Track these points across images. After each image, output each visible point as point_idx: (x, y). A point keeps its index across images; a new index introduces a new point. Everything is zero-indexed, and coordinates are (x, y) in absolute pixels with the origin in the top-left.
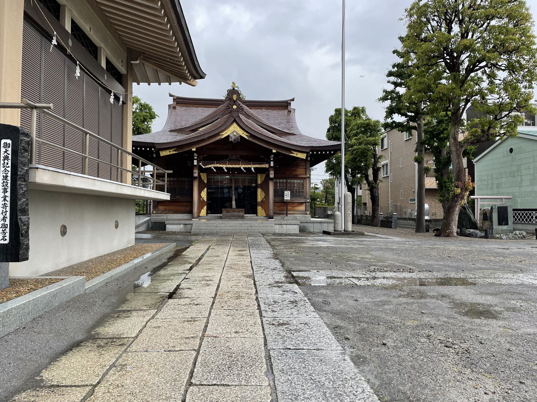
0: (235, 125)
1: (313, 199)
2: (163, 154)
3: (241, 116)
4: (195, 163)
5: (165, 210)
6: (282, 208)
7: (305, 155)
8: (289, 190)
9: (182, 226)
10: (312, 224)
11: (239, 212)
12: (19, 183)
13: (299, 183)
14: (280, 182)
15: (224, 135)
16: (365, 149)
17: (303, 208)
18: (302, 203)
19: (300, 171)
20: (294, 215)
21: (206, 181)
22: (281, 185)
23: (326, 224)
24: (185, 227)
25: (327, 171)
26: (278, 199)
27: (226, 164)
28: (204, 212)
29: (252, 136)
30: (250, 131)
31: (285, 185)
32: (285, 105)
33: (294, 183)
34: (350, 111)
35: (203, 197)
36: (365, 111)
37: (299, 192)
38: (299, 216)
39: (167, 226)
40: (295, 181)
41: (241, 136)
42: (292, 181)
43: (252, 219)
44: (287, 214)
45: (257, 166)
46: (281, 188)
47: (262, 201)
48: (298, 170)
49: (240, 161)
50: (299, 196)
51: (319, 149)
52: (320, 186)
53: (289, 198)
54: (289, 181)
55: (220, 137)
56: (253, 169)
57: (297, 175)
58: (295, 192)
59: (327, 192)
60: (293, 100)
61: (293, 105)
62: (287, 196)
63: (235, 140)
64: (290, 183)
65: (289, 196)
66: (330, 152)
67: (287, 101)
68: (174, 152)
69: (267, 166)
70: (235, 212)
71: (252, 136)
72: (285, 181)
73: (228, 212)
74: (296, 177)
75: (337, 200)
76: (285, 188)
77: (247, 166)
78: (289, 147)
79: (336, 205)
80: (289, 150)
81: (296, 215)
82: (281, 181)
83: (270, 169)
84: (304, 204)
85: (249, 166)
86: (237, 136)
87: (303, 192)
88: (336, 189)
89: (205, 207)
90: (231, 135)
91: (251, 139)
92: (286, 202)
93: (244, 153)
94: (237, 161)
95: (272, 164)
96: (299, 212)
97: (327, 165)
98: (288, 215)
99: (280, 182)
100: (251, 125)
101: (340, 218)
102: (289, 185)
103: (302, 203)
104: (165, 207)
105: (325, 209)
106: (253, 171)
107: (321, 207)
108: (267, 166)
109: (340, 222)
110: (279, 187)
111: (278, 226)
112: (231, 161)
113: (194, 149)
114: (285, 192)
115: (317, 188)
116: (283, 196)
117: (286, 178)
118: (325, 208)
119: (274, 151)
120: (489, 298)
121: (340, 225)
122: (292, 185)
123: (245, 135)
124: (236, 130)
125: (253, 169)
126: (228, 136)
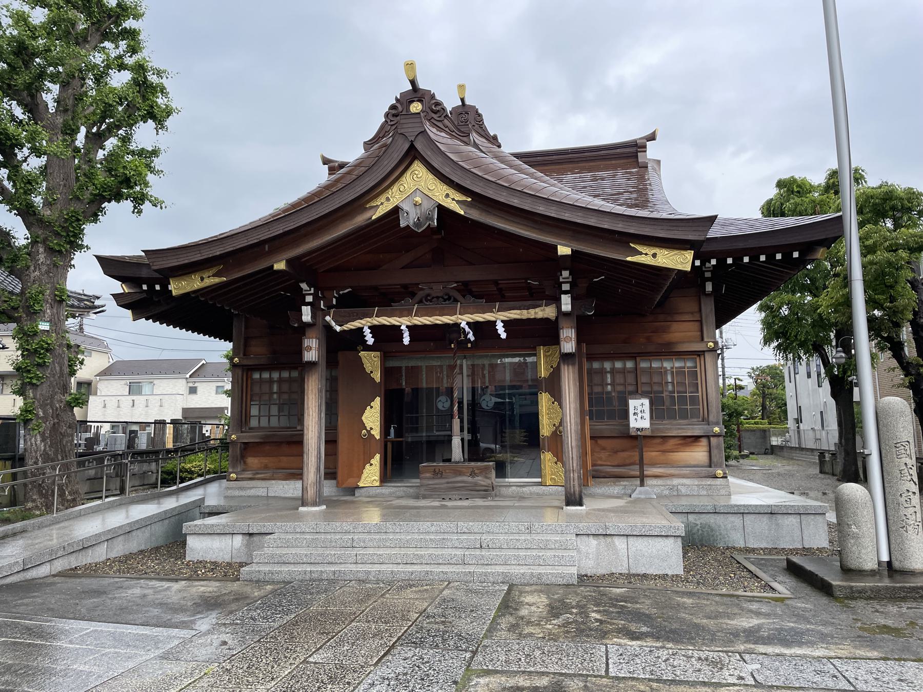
0: (418, 168)
1: (732, 415)
2: (177, 287)
3: (432, 132)
4: (307, 314)
5: (266, 467)
6: (618, 455)
7: (689, 255)
8: (644, 395)
9: (238, 541)
10: (737, 520)
11: (473, 474)
13: (680, 372)
14: (613, 371)
15: (381, 207)
16: (890, 264)
17: (699, 454)
18: (697, 438)
19: (681, 332)
20: (669, 482)
21: (377, 376)
22: (619, 379)
23: (793, 520)
24: (248, 546)
25: (767, 341)
26: (607, 426)
27: (409, 314)
28: (371, 473)
29: (479, 200)
30: (467, 184)
31: (630, 379)
32: (628, 156)
33: (662, 372)
34: (819, 185)
35: (368, 425)
36: (862, 177)
37: (683, 400)
38: (686, 485)
39: (191, 542)
40: (667, 365)
41: (441, 208)
42: (655, 365)
43: (522, 498)
44: (642, 478)
45: (514, 314)
48: (675, 326)
49: (456, 301)
50: (684, 415)
51: (741, 245)
52: (749, 384)
53: (645, 423)
54: (644, 365)
55: (366, 216)
56: (500, 328)
57: (669, 344)
58: (667, 402)
59: (764, 396)
60: (652, 137)
61: (652, 152)
62: (640, 415)
63: (418, 224)
64: (650, 371)
65: (647, 415)
66: (787, 256)
67: (635, 141)
68: (217, 280)
69: (547, 312)
70: (461, 473)
71: (479, 200)
72: (630, 364)
73: (437, 474)
74: (668, 351)
75: (792, 413)
76: (631, 388)
77: (479, 317)
78: (620, 227)
79: (791, 424)
80: (624, 240)
81: (676, 481)
82: (618, 365)
83: (562, 322)
84: (704, 442)
85: (489, 317)
86: (427, 205)
87: (694, 401)
88: (789, 387)
89: (376, 460)
90: (406, 207)
91: (475, 215)
93: (469, 274)
94: (447, 302)
95: (566, 303)
96: (686, 471)
97: (767, 325)
98: (649, 482)
100: (468, 159)
101: (865, 515)
102: (644, 379)
103: (697, 438)
104: (265, 460)
105: (765, 434)
106: (503, 336)
107: (753, 431)
108: (547, 312)
109: (866, 529)
111: (593, 542)
112: (429, 303)
113: (280, 266)
114: (633, 403)
115: (741, 388)
116: (625, 414)
117: (633, 357)
118: (764, 431)
119: (564, 250)
121: (868, 542)
122: (656, 379)
123: (453, 202)
124: (422, 186)
125: (500, 328)
126: (396, 210)
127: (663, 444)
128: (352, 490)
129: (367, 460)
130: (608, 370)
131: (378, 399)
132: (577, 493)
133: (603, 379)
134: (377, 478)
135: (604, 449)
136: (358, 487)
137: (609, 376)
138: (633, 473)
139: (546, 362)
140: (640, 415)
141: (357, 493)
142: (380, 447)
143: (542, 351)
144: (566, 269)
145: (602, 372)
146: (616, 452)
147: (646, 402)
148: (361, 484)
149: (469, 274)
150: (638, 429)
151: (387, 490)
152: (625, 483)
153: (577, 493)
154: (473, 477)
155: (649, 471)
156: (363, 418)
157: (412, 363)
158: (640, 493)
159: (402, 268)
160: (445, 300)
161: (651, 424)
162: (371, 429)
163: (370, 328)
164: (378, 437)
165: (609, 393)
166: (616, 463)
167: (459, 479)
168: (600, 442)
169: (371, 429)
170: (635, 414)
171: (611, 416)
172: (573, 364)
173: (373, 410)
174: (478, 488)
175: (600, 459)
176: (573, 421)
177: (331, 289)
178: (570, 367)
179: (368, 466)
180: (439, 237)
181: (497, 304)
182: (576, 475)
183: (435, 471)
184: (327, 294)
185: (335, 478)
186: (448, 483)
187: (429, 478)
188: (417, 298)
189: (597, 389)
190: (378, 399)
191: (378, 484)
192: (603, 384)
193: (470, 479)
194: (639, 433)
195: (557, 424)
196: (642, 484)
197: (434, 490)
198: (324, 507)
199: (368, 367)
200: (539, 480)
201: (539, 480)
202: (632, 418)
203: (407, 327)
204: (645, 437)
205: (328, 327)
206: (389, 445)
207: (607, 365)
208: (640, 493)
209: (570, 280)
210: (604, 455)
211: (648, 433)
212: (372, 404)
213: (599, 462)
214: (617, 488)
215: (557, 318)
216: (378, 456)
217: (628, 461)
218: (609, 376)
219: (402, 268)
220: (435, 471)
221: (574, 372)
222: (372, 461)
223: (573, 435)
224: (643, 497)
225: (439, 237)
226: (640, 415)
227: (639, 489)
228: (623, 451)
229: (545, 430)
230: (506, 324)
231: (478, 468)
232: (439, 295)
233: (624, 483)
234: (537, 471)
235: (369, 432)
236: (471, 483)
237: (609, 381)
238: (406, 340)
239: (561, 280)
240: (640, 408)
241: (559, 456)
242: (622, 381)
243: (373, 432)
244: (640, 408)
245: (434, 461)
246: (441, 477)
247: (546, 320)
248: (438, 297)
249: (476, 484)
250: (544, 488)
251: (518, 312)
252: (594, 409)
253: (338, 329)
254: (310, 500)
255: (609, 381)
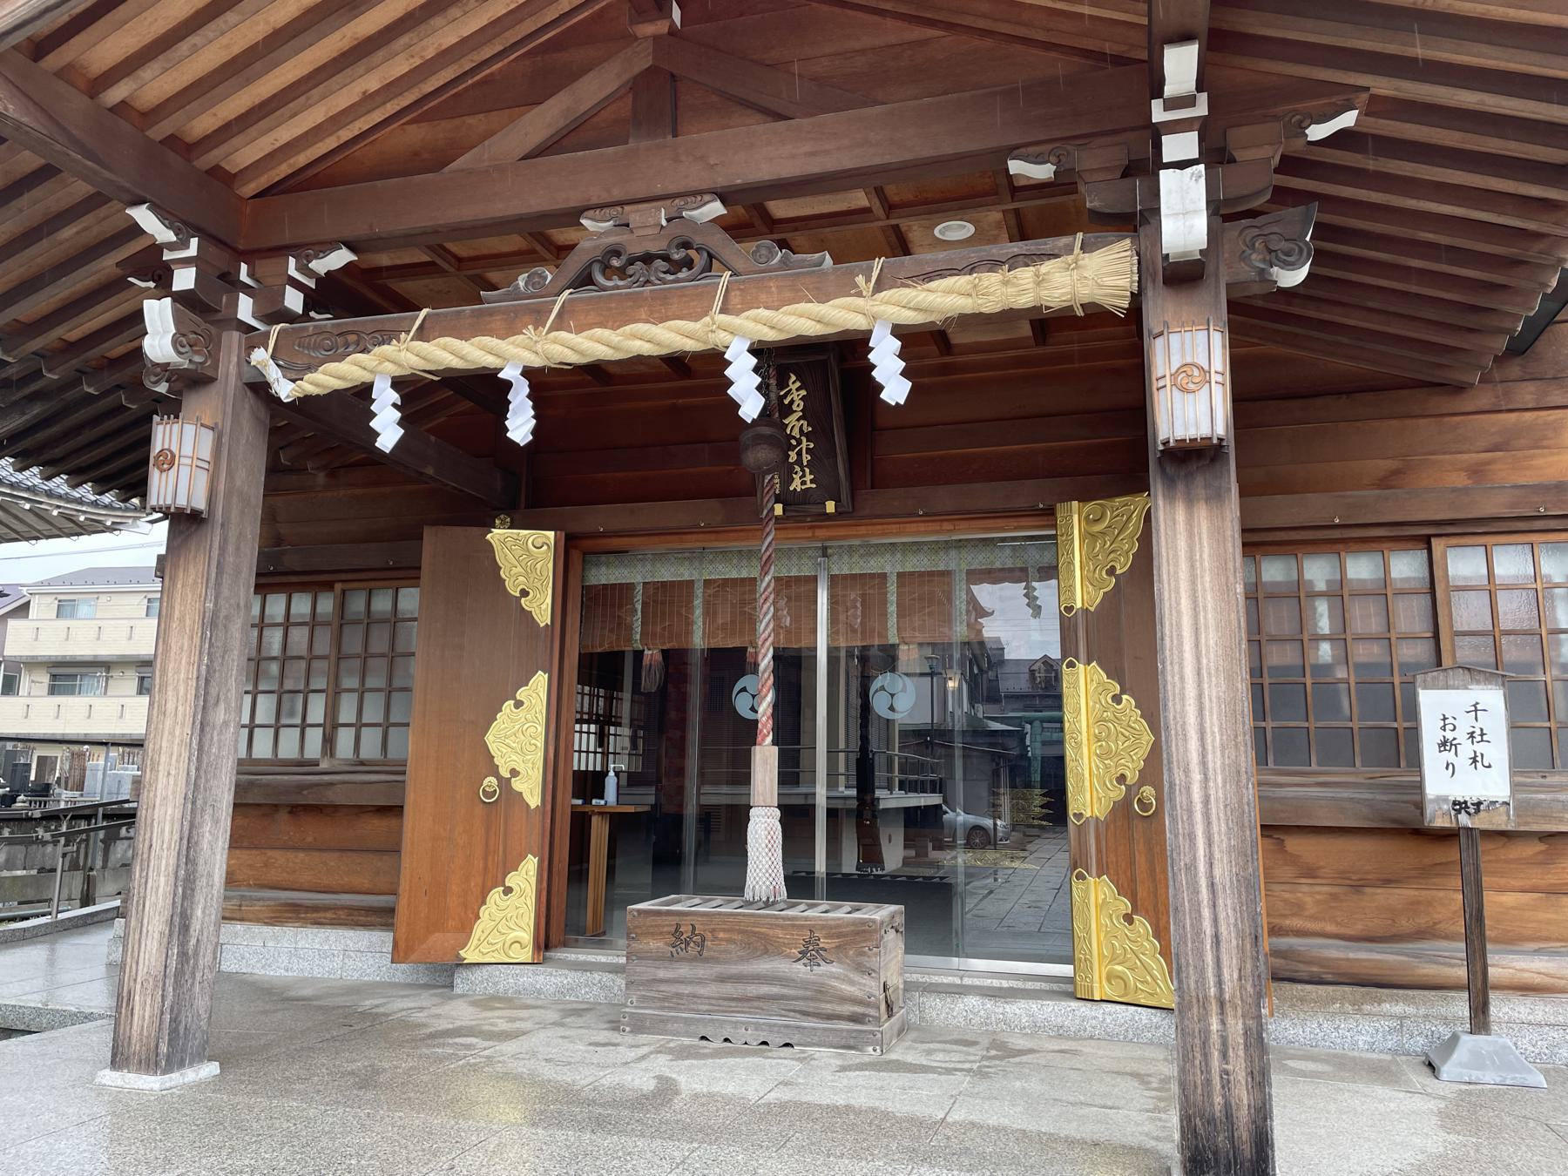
12: (854, 792)
14: (1339, 593)
21: (541, 608)
26: (1329, 791)
28: (509, 915)
46: (1364, 653)
47: (1122, 810)
65: (1498, 751)
69: (1092, 275)
72: (1406, 566)
82: (1361, 568)
83: (1157, 311)
89: (526, 876)
92: (1448, 836)
93: (769, 153)
95: (1184, 212)
99: (1339, 593)
108: (1092, 275)
110: (1340, 638)
114: (1437, 705)
116: (1401, 745)
117: (1422, 536)
120: (734, 575)
127: (1546, 861)
128: (446, 972)
129: (495, 875)
130: (1321, 586)
131: (540, 681)
132: (1243, 1117)
133: (1302, 619)
134: (527, 936)
135: (1310, 872)
136: (461, 965)
137: (1322, 607)
138: (1428, 970)
139: (1090, 556)
140: (1466, 749)
141: (462, 982)
142: (535, 833)
143: (1074, 517)
144: (1183, 38)
145: (1299, 594)
146: (1358, 887)
147: (1492, 698)
148: (469, 955)
149: (769, 153)
150: (1460, 806)
151: (551, 980)
152: (1398, 1009)
153: (1243, 1117)
154: (813, 962)
155: (1501, 966)
156: (490, 738)
157: (667, 573)
158: (1478, 1061)
159: (523, 158)
160: (676, 267)
161: (1515, 787)
162: (514, 773)
163: (397, 384)
164: (534, 800)
165: (1327, 668)
166: (1358, 928)
167: (764, 966)
168: (1293, 844)
169: (514, 773)
170: (1444, 744)
171: (1339, 747)
172: (1216, 498)
173: (522, 712)
174: (828, 1008)
175: (1298, 908)
176: (1215, 761)
177: (282, 251)
178: (1202, 513)
179: (496, 895)
180: (661, 27)
181: (878, 264)
182: (1236, 1027)
183: (677, 932)
184: (267, 266)
185: (388, 926)
186: (722, 979)
187: (659, 958)
188: (574, 264)
189: (1278, 656)
190: (540, 681)
191: (526, 954)
192: (1303, 638)
193: (800, 970)
194: (1464, 820)
195: (1132, 777)
196: (1480, 1019)
197: (676, 1002)
198: (211, 1069)
199: (513, 578)
200: (1066, 970)
201: (1066, 970)
202: (1432, 759)
203: (527, 373)
204: (1489, 835)
205: (260, 388)
206: (599, 831)
207: (1318, 571)
208: (1478, 1061)
209: (1201, 109)
210: (1310, 894)
211: (1500, 822)
212: (521, 694)
213: (1296, 923)
214: (1366, 1026)
215: (1136, 298)
216: (530, 865)
217: (1405, 925)
218: (1322, 607)
219: (523, 158)
220: (677, 932)
221: (1218, 534)
222: (512, 880)
223: (1219, 828)
224: (1489, 1077)
225: (661, 27)
226: (1466, 749)
227: (1468, 1042)
228: (1387, 882)
229: (1090, 794)
230: (912, 340)
231: (835, 931)
232: (653, 248)
233: (1397, 1005)
234: (1054, 936)
235: (505, 784)
236: (805, 984)
237: (1324, 625)
238: (520, 425)
239: (1159, 114)
240: (1465, 724)
241: (1149, 890)
242: (1375, 625)
243: (517, 785)
244: (1465, 724)
245: (676, 888)
246: (700, 958)
247: (1096, 315)
248: (647, 259)
249: (820, 992)
250: (1084, 1009)
251: (962, 281)
252: (1269, 724)
253: (285, 390)
254: (136, 1046)
255: (1324, 625)
